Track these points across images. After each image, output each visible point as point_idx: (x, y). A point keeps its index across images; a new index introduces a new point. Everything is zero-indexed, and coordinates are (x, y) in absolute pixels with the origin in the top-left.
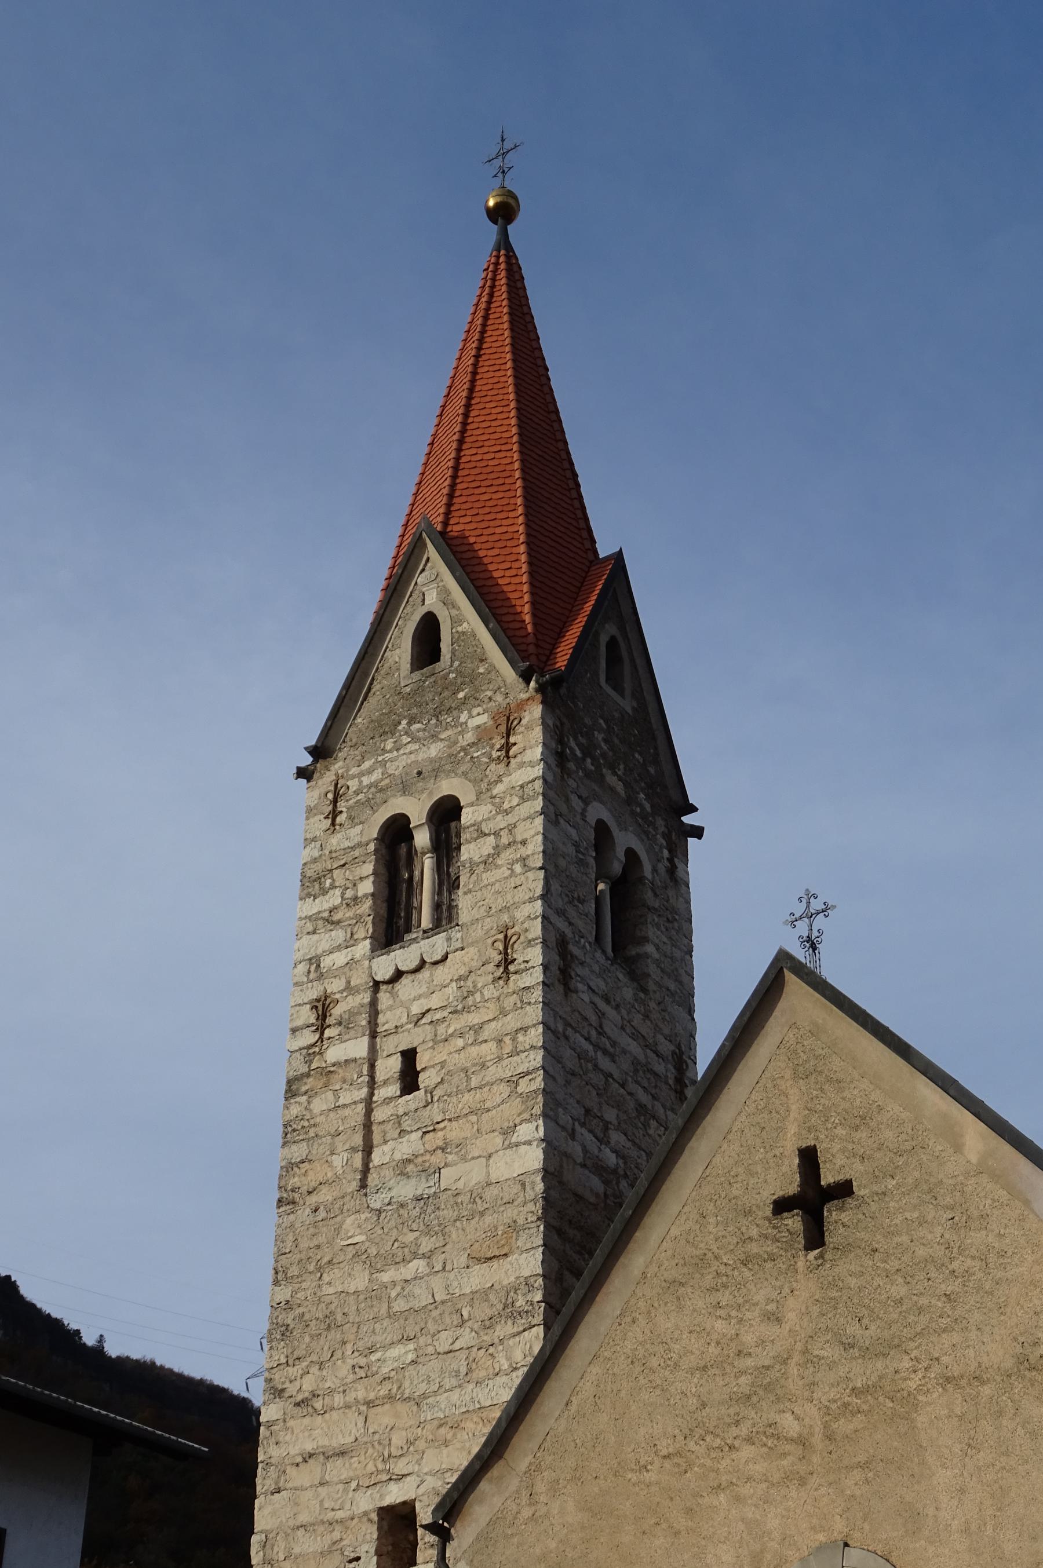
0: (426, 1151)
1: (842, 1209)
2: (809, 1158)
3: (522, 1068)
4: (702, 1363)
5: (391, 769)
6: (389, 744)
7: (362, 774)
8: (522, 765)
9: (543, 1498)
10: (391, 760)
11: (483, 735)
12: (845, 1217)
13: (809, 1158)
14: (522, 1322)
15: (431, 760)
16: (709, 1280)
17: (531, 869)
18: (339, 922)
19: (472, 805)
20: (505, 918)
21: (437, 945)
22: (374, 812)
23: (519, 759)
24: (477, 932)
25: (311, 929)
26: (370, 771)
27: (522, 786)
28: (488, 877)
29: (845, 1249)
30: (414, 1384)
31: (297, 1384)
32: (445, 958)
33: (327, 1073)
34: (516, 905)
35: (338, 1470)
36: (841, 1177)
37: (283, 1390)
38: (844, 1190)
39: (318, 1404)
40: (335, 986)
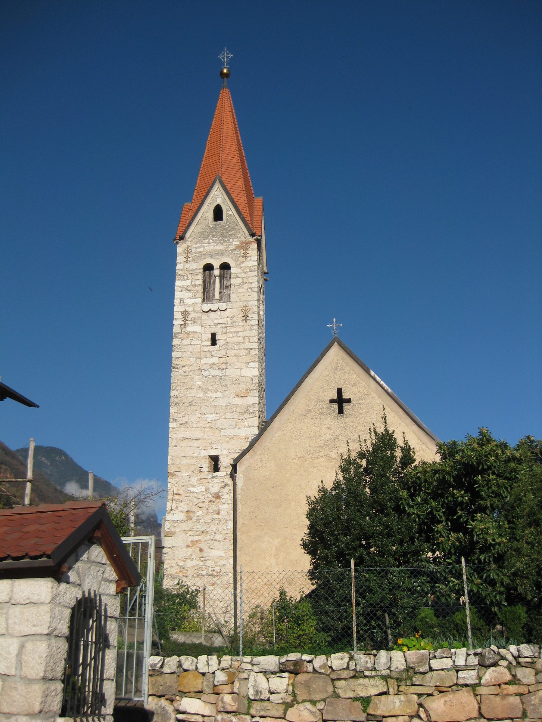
0: (219, 363)
1: (348, 405)
2: (340, 391)
4: (310, 436)
5: (207, 249)
6: (206, 241)
7: (196, 248)
8: (250, 260)
9: (264, 462)
10: (207, 246)
11: (237, 248)
13: (340, 391)
14: (252, 415)
15: (220, 250)
16: (312, 416)
17: (254, 292)
18: (190, 290)
19: (234, 267)
20: (245, 303)
21: (223, 306)
22: (202, 261)
23: (249, 258)
25: (180, 290)
26: (199, 247)
27: (251, 266)
28: (240, 290)
29: (350, 415)
30: (219, 425)
31: (181, 419)
32: (226, 309)
33: (188, 334)
34: (249, 301)
35: (195, 443)
36: (349, 397)
37: (176, 420)
38: (349, 401)
39: (188, 425)
40: (190, 309)
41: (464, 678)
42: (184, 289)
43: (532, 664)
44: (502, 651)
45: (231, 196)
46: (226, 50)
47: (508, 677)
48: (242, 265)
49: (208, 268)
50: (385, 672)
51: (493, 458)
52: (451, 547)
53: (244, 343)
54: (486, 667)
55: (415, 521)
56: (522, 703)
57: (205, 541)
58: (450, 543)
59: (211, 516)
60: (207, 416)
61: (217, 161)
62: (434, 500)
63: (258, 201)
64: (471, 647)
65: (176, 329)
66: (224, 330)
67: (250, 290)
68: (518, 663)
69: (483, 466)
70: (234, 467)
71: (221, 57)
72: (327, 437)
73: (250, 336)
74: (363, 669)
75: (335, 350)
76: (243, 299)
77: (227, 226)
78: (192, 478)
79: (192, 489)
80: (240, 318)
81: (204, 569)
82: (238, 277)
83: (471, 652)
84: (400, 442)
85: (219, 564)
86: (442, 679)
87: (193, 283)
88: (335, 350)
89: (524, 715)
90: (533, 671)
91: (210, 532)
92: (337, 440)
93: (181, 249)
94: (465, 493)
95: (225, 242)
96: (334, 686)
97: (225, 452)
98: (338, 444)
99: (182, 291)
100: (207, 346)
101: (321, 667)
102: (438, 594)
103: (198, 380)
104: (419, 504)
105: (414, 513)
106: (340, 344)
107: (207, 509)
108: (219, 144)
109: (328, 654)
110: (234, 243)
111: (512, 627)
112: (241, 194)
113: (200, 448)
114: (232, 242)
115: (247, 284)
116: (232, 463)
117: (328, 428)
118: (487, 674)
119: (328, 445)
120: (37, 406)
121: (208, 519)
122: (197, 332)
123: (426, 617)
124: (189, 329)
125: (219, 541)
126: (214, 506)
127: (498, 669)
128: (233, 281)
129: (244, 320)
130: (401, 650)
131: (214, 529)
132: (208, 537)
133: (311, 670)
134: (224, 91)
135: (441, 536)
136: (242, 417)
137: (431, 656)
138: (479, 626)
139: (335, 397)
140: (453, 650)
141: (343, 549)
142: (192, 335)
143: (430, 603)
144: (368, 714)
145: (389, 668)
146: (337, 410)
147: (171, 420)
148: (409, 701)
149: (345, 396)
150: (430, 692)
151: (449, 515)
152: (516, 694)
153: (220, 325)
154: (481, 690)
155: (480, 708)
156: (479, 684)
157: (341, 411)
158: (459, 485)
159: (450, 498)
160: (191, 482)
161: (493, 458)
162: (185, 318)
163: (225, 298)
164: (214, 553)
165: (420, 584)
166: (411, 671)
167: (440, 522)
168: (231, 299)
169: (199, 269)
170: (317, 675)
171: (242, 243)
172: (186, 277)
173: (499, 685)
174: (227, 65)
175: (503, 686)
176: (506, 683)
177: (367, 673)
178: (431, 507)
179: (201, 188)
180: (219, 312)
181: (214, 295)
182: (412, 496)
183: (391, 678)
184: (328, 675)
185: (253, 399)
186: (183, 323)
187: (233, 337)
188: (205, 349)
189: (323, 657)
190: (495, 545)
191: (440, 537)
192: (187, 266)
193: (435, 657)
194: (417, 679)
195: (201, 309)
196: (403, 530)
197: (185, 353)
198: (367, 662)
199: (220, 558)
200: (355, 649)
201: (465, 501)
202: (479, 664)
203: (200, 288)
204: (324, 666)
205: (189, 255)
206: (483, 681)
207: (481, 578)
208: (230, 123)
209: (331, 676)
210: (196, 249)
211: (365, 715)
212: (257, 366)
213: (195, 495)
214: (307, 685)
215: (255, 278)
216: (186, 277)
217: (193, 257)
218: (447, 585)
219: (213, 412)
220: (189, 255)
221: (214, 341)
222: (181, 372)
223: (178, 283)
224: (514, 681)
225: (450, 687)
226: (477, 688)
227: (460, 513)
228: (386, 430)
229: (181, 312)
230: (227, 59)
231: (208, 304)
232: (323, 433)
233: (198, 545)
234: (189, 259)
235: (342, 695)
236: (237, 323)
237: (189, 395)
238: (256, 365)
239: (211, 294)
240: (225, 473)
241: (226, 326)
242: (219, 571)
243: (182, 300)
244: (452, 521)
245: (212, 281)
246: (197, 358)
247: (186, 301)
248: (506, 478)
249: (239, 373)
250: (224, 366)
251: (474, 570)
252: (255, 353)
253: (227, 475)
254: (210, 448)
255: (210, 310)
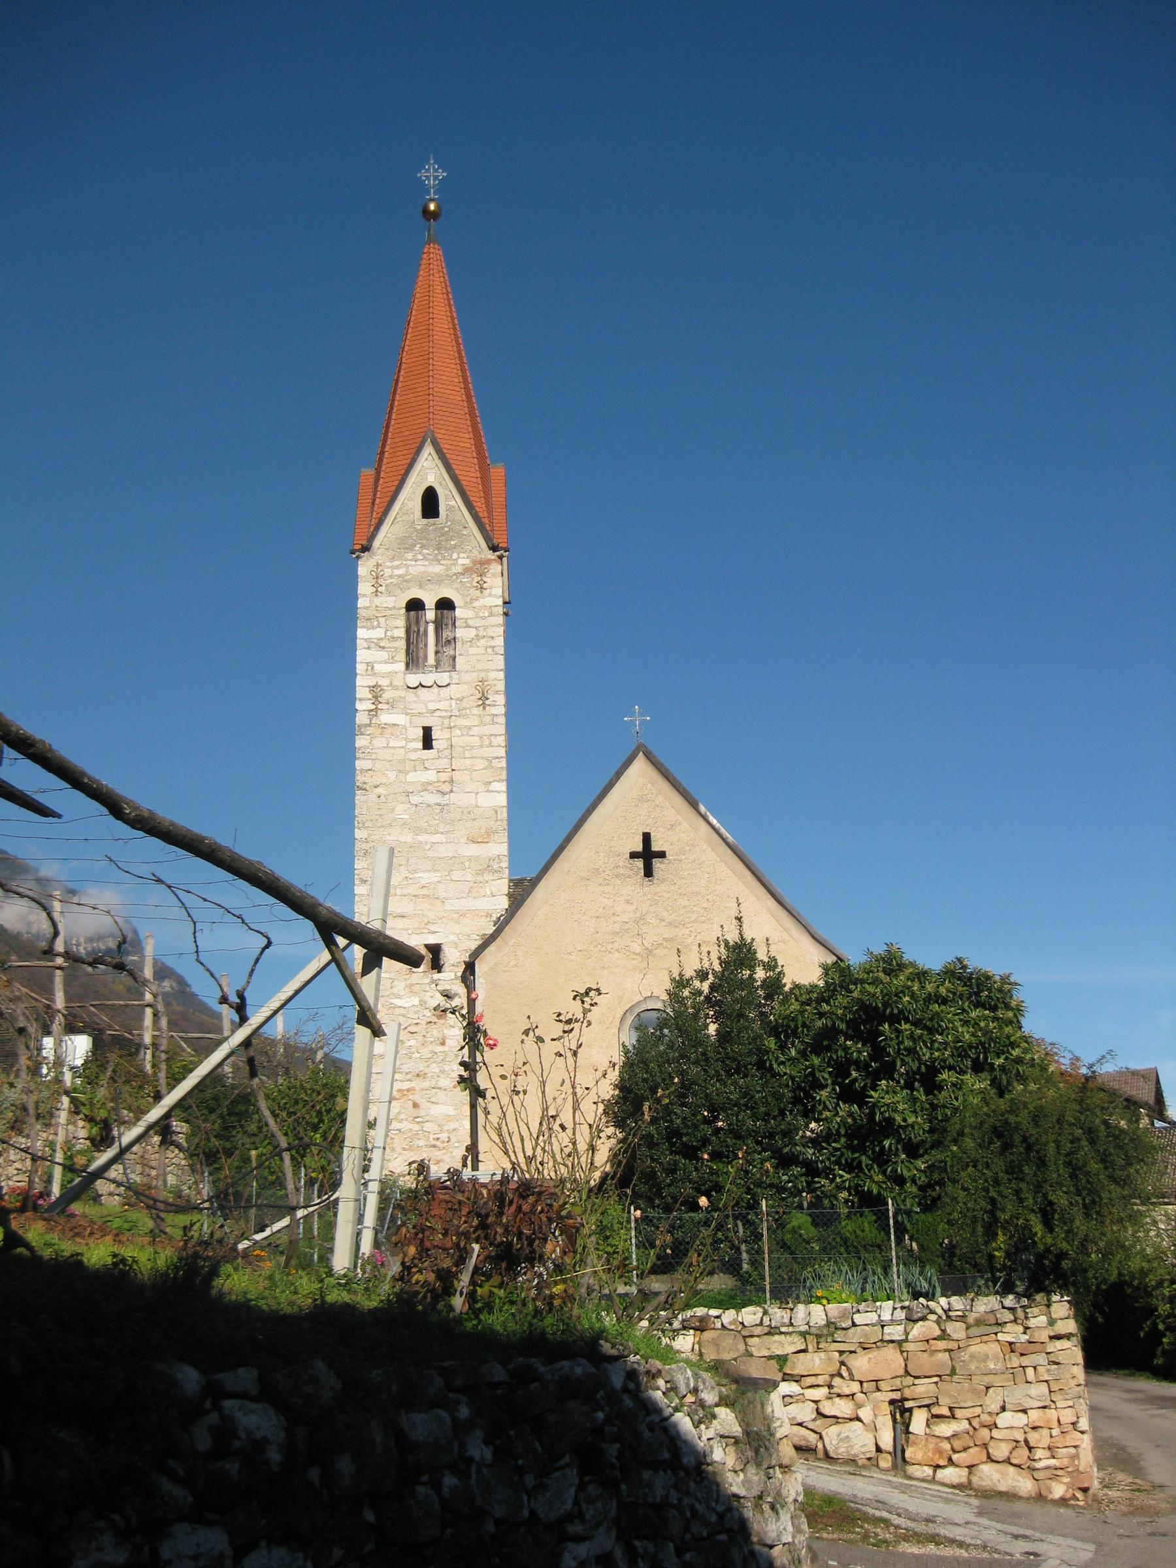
0: (438, 781)
2: (647, 838)
3: (495, 755)
6: (410, 555)
7: (392, 568)
8: (490, 595)
11: (467, 571)
12: (663, 866)
13: (647, 838)
15: (436, 574)
18: (383, 648)
20: (483, 674)
21: (444, 678)
23: (488, 591)
24: (467, 677)
26: (397, 567)
28: (473, 651)
29: (663, 881)
32: (448, 685)
33: (382, 728)
34: (488, 671)
38: (662, 855)
40: (384, 682)
41: (889, 1334)
42: (372, 645)
43: (962, 1318)
44: (930, 1303)
45: (476, 512)
46: (432, 162)
47: (938, 1332)
48: (476, 604)
49: (415, 606)
50: (804, 1328)
51: (907, 998)
52: (839, 1126)
53: (481, 746)
54: (913, 1321)
55: (787, 1086)
56: (952, 1359)
57: (422, 1090)
58: (838, 1119)
59: (430, 1047)
60: (419, 875)
61: (425, 397)
62: (818, 1055)
63: (498, 472)
64: (897, 1299)
65: (361, 718)
66: (446, 722)
67: (489, 650)
68: (948, 1317)
69: (892, 1009)
70: (470, 968)
71: (422, 174)
72: (625, 918)
73: (491, 735)
74: (778, 1325)
75: (639, 768)
76: (479, 667)
77: (446, 529)
78: (396, 983)
79: (397, 1002)
80: (472, 702)
81: (421, 1136)
82: (468, 626)
83: (898, 1305)
84: (761, 955)
85: (446, 1128)
86: (866, 1336)
87: (389, 634)
88: (639, 768)
89: (953, 1372)
90: (964, 1325)
91: (429, 1075)
92: (642, 922)
93: (364, 567)
94: (863, 1045)
95: (444, 558)
96: (746, 1345)
97: (452, 938)
98: (644, 929)
99: (369, 648)
100: (415, 750)
101: (731, 1323)
102: (819, 1193)
103: (401, 811)
104: (791, 1059)
105: (785, 1074)
106: (649, 757)
107: (424, 1036)
108: (426, 357)
109: (739, 1307)
110: (460, 561)
111: (925, 1243)
112: (470, 465)
113: (410, 932)
114: (456, 560)
115: (485, 639)
116: (467, 959)
117: (627, 902)
118: (915, 1329)
119: (627, 931)
120: (60, 816)
121: (425, 1052)
122: (398, 725)
123: (800, 1227)
124: (385, 718)
125: (445, 1090)
126: (435, 1032)
127: (927, 1323)
128: (460, 633)
129: (479, 705)
130: (821, 1304)
131: (437, 1070)
132: (426, 1084)
133: (720, 1327)
134: (432, 250)
135: (825, 1108)
136: (480, 879)
137: (854, 1310)
138: (878, 1242)
139: (639, 848)
140: (878, 1304)
141: (678, 1127)
142: (389, 730)
143: (805, 1205)
144: (785, 1374)
145: (808, 1323)
146: (642, 871)
147: (357, 882)
148: (830, 1359)
149: (655, 847)
150: (853, 1349)
151: (837, 1076)
152: (945, 1350)
153: (437, 713)
154: (908, 1346)
155: (906, 1365)
156: (906, 1340)
157: (648, 872)
158: (856, 1036)
159: (840, 1053)
160: (395, 991)
161: (907, 998)
162: (376, 698)
163: (445, 661)
164: (438, 1110)
165: (792, 1178)
166: (833, 1326)
167: (823, 1087)
168: (457, 666)
169: (400, 609)
170: (727, 1332)
171: (475, 562)
172: (376, 623)
173: (927, 1341)
174: (435, 193)
175: (932, 1342)
176: (935, 1339)
177: (783, 1329)
178: (812, 1066)
179: (397, 449)
180: (435, 689)
181: (426, 657)
182: (783, 1047)
183: (810, 1334)
184: (739, 1332)
185: (499, 848)
186: (374, 707)
187: (462, 735)
188: (414, 756)
189: (732, 1312)
190: (906, 1127)
191: (824, 1109)
192: (377, 601)
193: (858, 1311)
194: (839, 1336)
195: (405, 682)
196: (769, 1099)
197: (378, 762)
198: (783, 1317)
199: (448, 1118)
200: (768, 1302)
201: (862, 1058)
202: (907, 1319)
203: (402, 644)
204: (734, 1322)
205: (381, 581)
206: (910, 1337)
207: (884, 1173)
208: (445, 318)
209: (743, 1333)
210: (393, 570)
211: (781, 1375)
212: (504, 788)
213: (403, 1011)
214: (715, 1343)
215: (498, 629)
216: (376, 623)
217: (386, 585)
218: (832, 1181)
219: (429, 868)
220: (381, 581)
221: (428, 742)
222: (372, 797)
223: (361, 633)
224: (944, 1336)
225: (875, 1343)
226: (904, 1344)
227: (854, 1074)
228: (742, 938)
229: (369, 687)
230: (434, 180)
231: (416, 673)
232: (618, 909)
233: (410, 1097)
234: (379, 589)
235: (755, 1353)
236: (468, 711)
237: (388, 837)
238: (503, 787)
239: (421, 655)
240: (452, 975)
241: (449, 714)
242: (447, 1139)
243: (370, 665)
244: (841, 1085)
245: (422, 629)
246: (400, 771)
247: (377, 667)
248: (925, 1027)
249: (473, 802)
250: (446, 788)
251: (873, 1161)
252: (500, 765)
253: (456, 978)
254: (425, 931)
255: (421, 685)
